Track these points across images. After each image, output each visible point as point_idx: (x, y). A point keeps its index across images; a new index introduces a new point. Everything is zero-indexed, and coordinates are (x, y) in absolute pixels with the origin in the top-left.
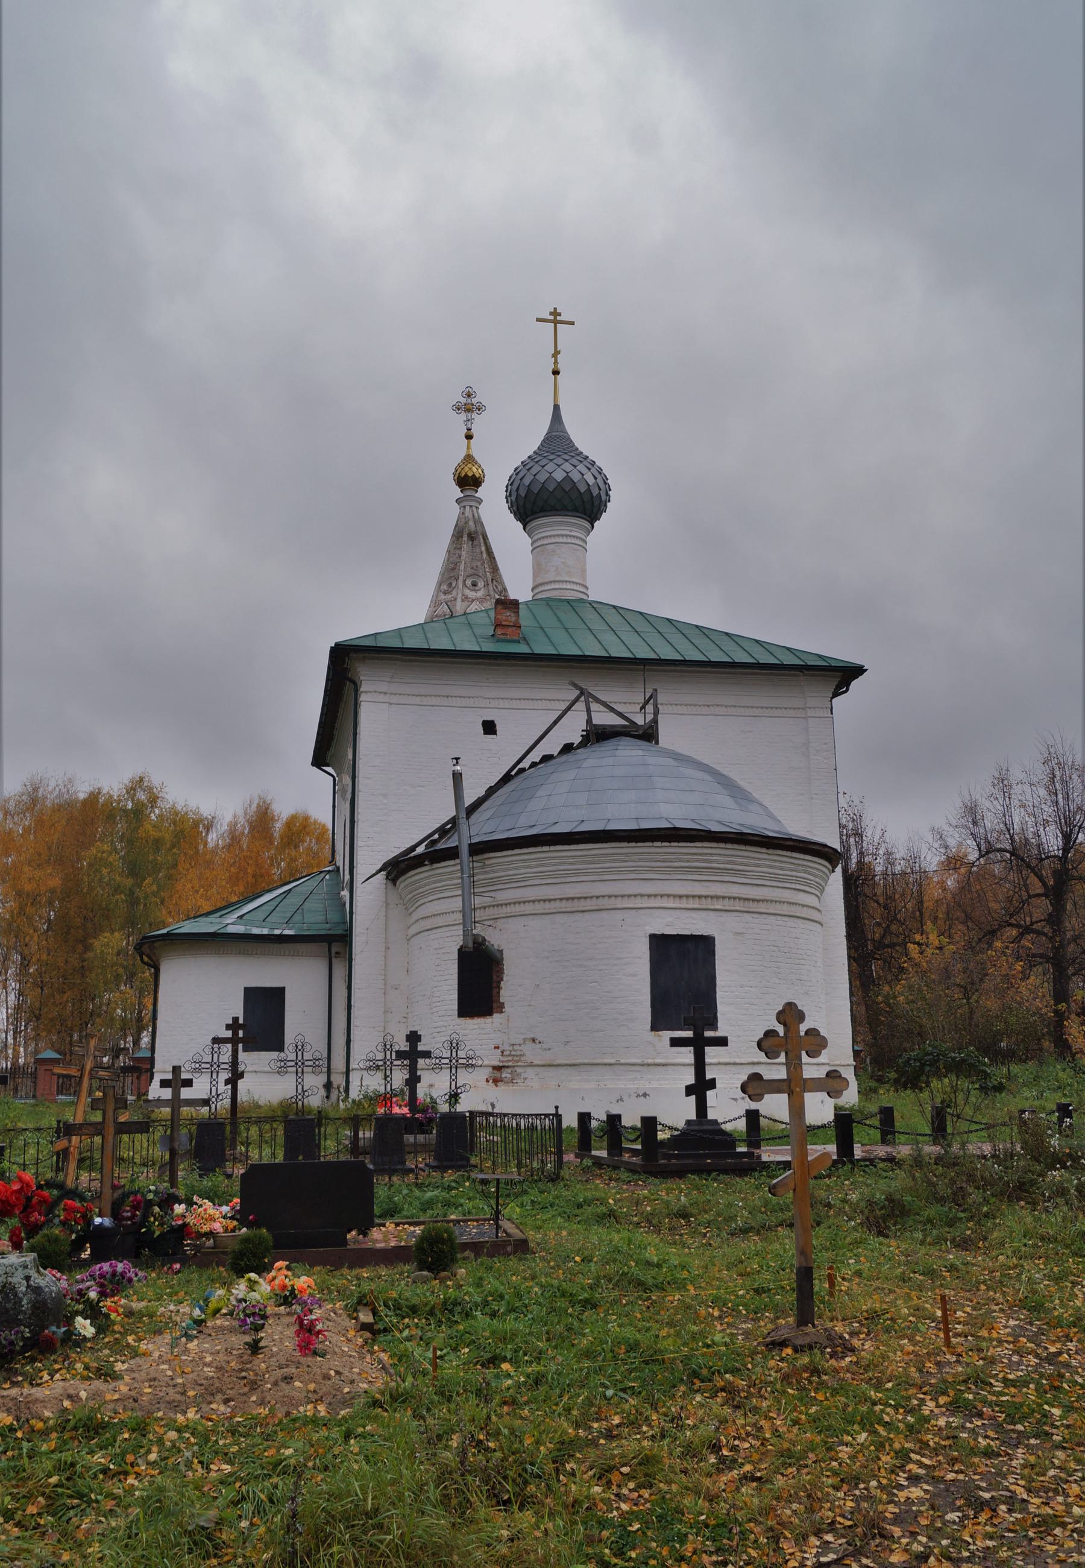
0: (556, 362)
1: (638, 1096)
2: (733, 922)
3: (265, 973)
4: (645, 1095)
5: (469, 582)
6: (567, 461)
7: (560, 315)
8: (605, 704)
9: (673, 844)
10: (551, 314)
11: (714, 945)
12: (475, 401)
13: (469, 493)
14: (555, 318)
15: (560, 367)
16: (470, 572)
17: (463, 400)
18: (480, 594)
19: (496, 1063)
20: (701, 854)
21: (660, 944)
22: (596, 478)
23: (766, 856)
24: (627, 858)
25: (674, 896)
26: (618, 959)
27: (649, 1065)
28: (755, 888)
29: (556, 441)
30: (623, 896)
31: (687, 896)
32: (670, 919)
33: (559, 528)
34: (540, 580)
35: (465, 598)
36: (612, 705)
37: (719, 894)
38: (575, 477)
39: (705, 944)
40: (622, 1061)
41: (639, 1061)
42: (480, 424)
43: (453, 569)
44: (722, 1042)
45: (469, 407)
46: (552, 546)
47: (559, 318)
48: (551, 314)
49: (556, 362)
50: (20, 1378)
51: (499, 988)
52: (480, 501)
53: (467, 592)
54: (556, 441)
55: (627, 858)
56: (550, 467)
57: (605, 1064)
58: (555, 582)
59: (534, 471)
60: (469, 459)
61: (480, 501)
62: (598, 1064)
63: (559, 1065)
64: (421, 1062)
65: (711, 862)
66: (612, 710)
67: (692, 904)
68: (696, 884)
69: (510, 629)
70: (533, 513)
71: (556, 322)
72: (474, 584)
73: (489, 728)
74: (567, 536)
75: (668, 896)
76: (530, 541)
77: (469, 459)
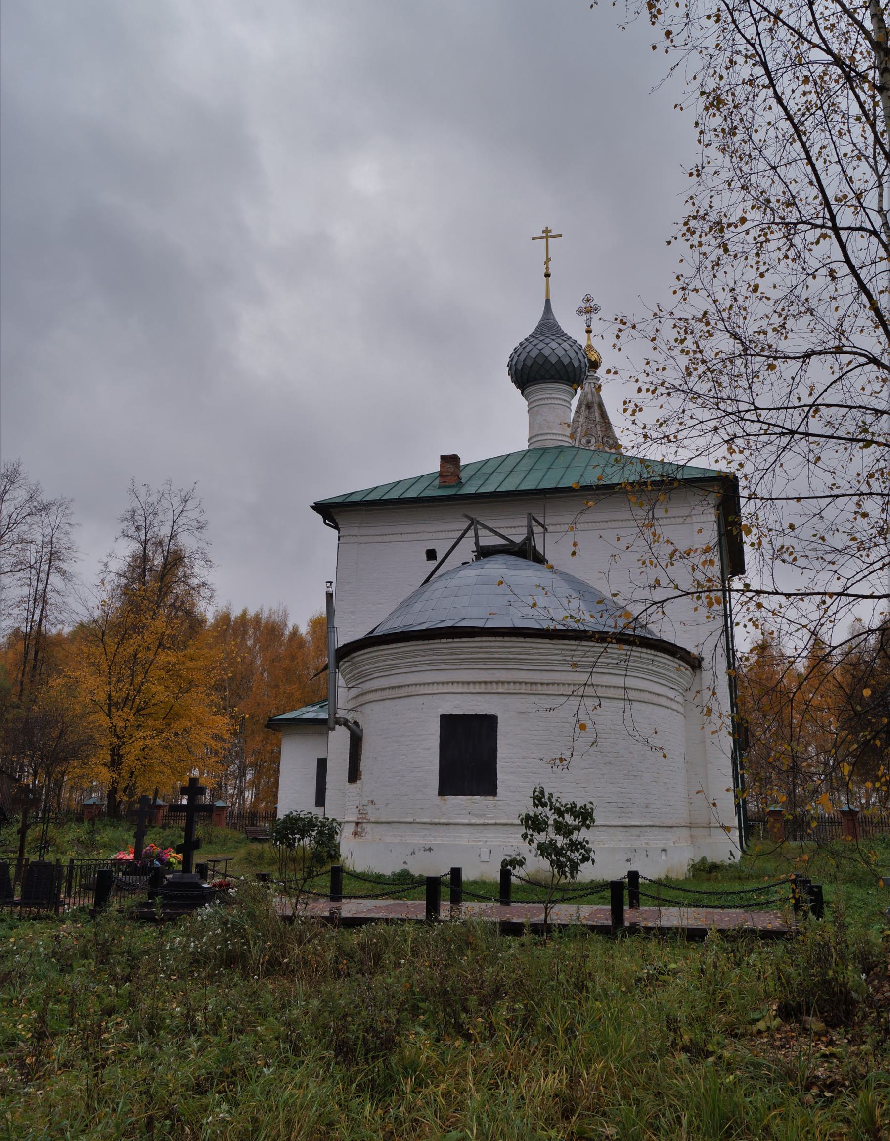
0: (547, 268)
1: (425, 850)
2: (517, 703)
4: (430, 849)
7: (550, 231)
8: (491, 530)
9: (456, 640)
10: (544, 232)
11: (497, 723)
12: (592, 304)
14: (547, 235)
15: (550, 271)
17: (584, 305)
19: (356, 820)
20: (481, 647)
21: (448, 723)
23: (552, 646)
24: (424, 654)
25: (463, 683)
26: (419, 735)
27: (436, 824)
28: (544, 673)
29: (548, 326)
30: (424, 684)
31: (474, 683)
32: (458, 702)
36: (498, 530)
37: (502, 680)
38: (547, 352)
39: (488, 723)
40: (418, 820)
41: (428, 820)
46: (536, 408)
47: (549, 234)
48: (544, 232)
49: (547, 268)
54: (548, 326)
55: (424, 654)
57: (407, 823)
58: (539, 435)
59: (527, 350)
62: (402, 823)
63: (381, 823)
65: (492, 653)
66: (496, 533)
67: (478, 688)
68: (483, 671)
69: (449, 478)
71: (547, 238)
74: (547, 398)
75: (458, 683)
76: (526, 403)
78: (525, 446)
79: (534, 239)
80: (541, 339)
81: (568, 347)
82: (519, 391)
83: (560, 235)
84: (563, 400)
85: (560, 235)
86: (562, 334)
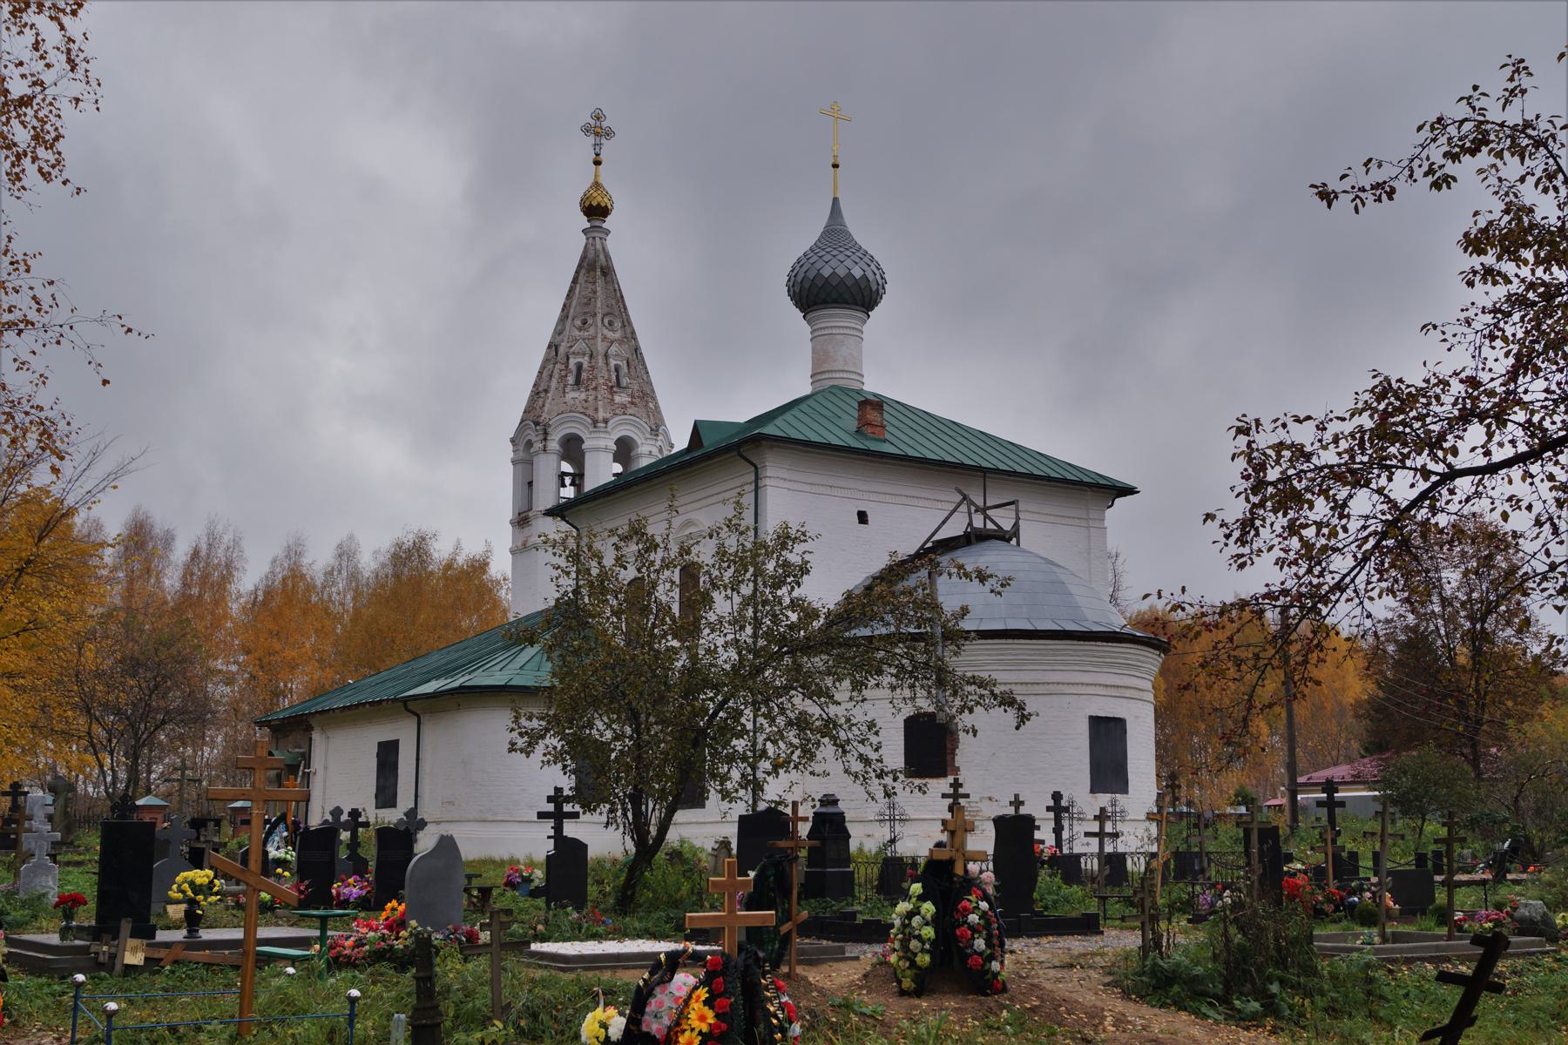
3: (385, 733)
5: (578, 323)
12: (604, 124)
13: (597, 223)
16: (606, 310)
18: (618, 335)
29: (835, 232)
33: (839, 320)
35: (605, 338)
43: (587, 304)
44: (944, 796)
50: (1255, 1006)
51: (953, 754)
52: (607, 232)
53: (605, 331)
54: (835, 232)
56: (834, 263)
60: (597, 185)
61: (607, 232)
64: (1338, 810)
70: (815, 303)
72: (611, 323)
73: (863, 517)
77: (597, 185)
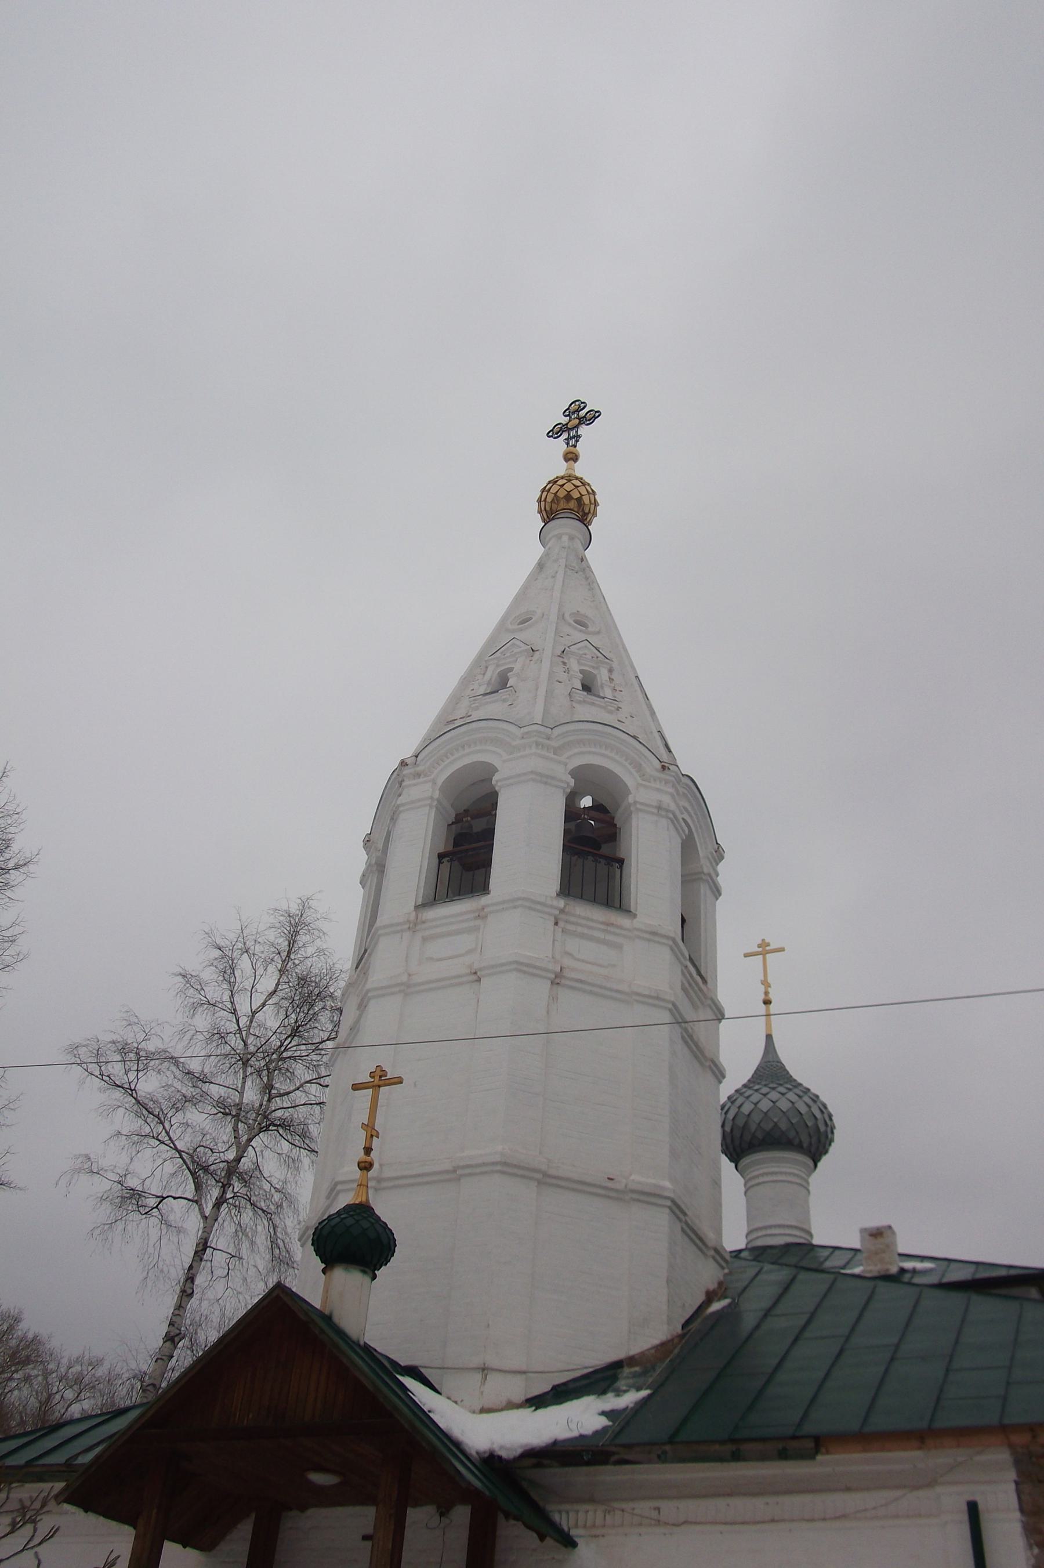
6: (774, 1089)
14: (764, 949)
15: (771, 996)
22: (809, 1107)
34: (751, 1228)
42: (762, 996)
45: (577, 418)
48: (759, 946)
59: (738, 1103)
76: (742, 1181)
78: (743, 1246)
79: (746, 955)
80: (757, 1087)
81: (584, 492)
82: (733, 1165)
83: (782, 950)
84: (790, 1174)
85: (782, 950)
86: (789, 1079)
